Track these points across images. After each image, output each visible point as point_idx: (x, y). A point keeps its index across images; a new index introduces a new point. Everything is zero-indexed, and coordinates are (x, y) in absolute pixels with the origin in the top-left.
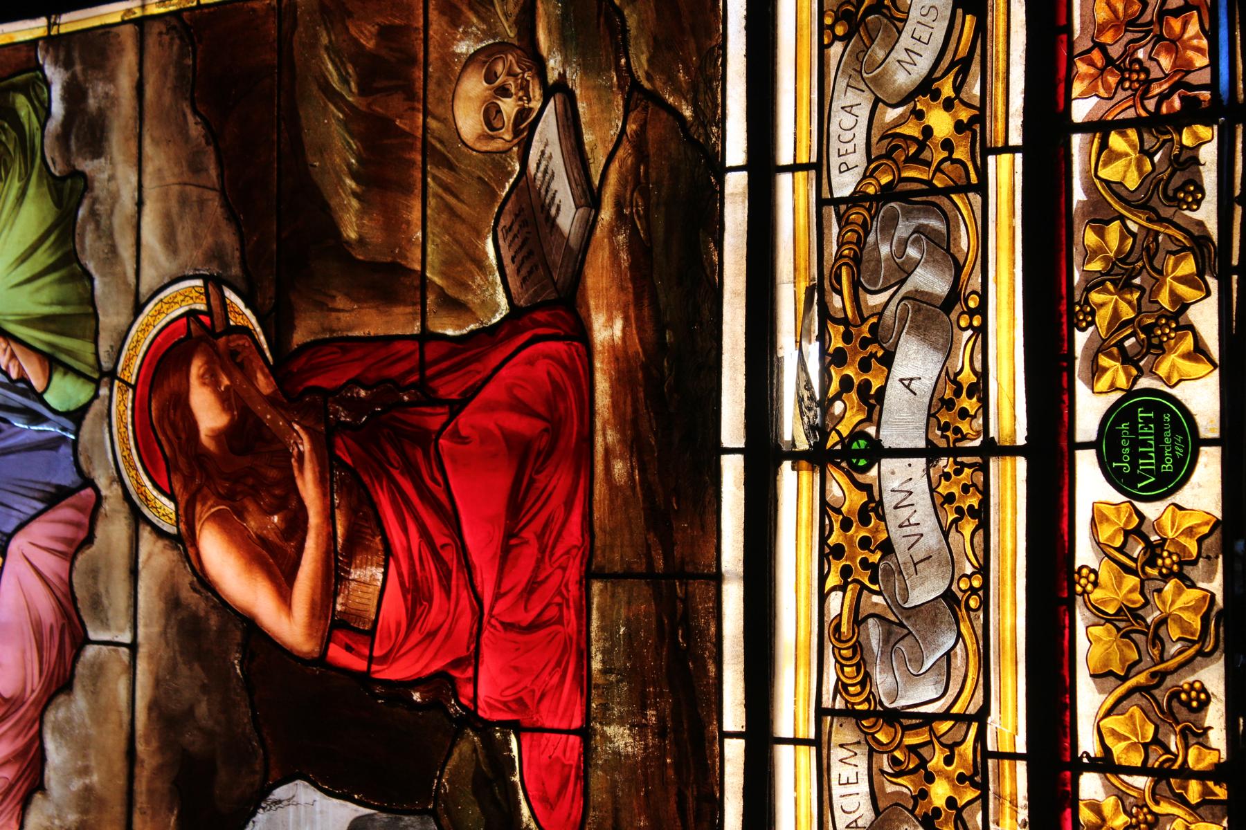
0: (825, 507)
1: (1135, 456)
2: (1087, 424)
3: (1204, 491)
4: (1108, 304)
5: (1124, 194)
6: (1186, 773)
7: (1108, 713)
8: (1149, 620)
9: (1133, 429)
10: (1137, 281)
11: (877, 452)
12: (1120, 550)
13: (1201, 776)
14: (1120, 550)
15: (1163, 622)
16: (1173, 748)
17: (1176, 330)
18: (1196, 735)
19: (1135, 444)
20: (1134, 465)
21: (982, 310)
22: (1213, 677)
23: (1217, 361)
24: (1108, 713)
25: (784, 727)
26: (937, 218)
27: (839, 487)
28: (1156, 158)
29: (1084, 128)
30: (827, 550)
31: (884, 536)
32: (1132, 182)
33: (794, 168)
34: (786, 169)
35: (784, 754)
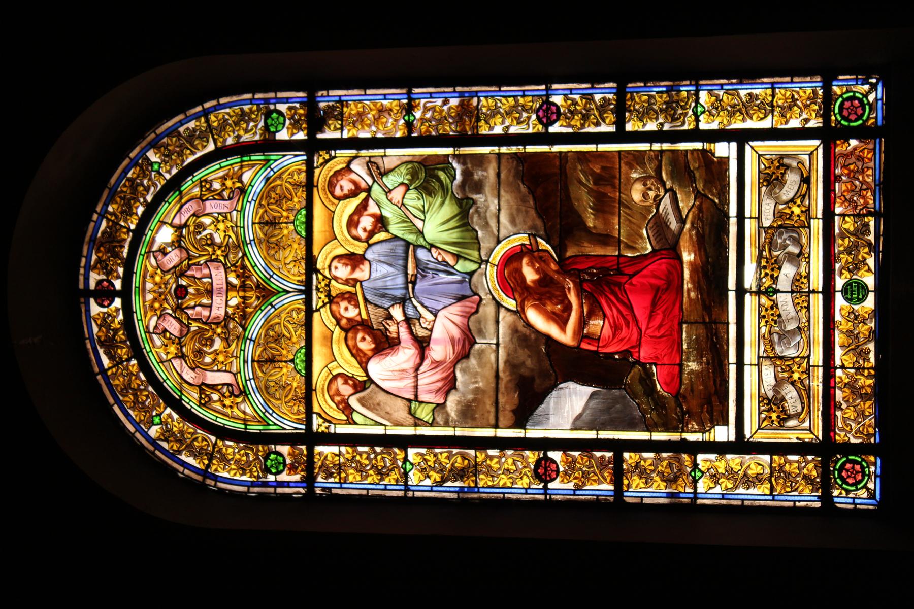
3: (870, 303)
6: (864, 369)
18: (867, 360)
22: (871, 346)
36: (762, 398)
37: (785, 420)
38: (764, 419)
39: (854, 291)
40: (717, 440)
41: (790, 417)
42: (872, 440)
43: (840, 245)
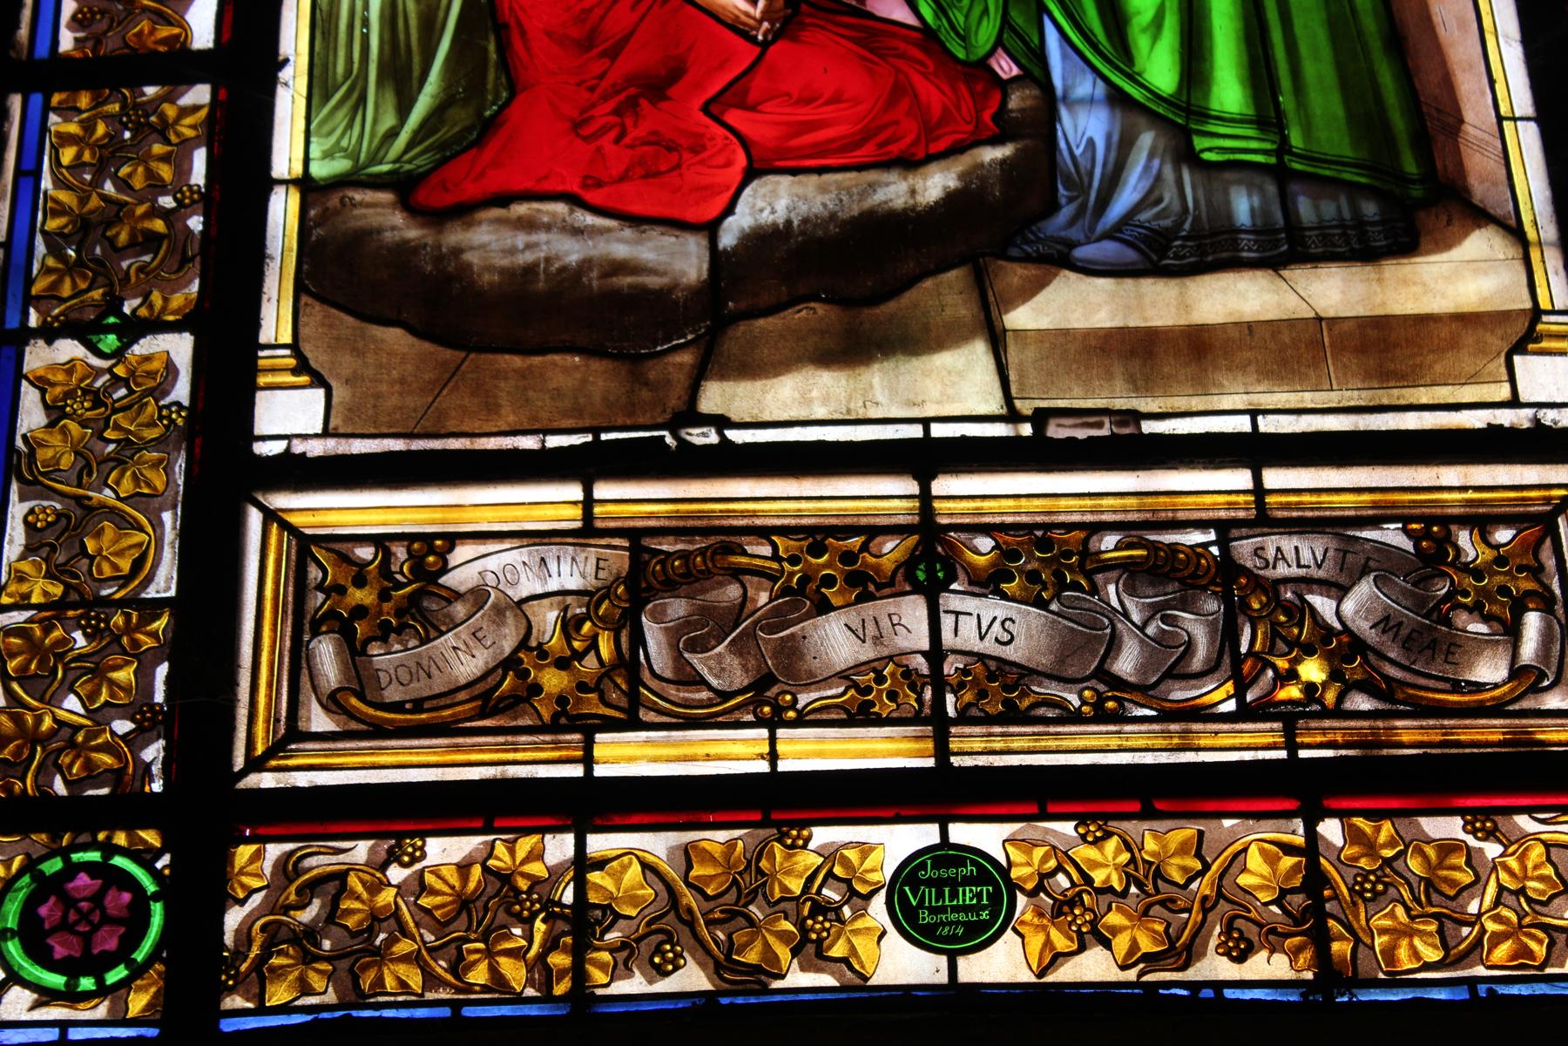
1: (938, 884)
3: (902, 963)
4: (1106, 862)
5: (1233, 870)
6: (579, 953)
7: (645, 866)
8: (751, 907)
9: (968, 881)
10: (1133, 890)
11: (932, 593)
12: (830, 874)
13: (579, 973)
14: (830, 874)
15: (751, 922)
16: (607, 937)
17: (1079, 932)
18: (625, 957)
19: (954, 884)
20: (930, 883)
21: (1101, 716)
22: (692, 978)
23: (1049, 979)
24: (645, 866)
26: (1207, 660)
28: (1274, 908)
29: (1311, 834)
30: (819, 538)
31: (836, 601)
32: (1244, 880)
33: (926, 497)
34: (1257, 479)
36: (433, 548)
37: (345, 632)
38: (345, 559)
39: (943, 901)
40: (261, 397)
41: (354, 652)
42: (236, 1002)
43: (1164, 840)
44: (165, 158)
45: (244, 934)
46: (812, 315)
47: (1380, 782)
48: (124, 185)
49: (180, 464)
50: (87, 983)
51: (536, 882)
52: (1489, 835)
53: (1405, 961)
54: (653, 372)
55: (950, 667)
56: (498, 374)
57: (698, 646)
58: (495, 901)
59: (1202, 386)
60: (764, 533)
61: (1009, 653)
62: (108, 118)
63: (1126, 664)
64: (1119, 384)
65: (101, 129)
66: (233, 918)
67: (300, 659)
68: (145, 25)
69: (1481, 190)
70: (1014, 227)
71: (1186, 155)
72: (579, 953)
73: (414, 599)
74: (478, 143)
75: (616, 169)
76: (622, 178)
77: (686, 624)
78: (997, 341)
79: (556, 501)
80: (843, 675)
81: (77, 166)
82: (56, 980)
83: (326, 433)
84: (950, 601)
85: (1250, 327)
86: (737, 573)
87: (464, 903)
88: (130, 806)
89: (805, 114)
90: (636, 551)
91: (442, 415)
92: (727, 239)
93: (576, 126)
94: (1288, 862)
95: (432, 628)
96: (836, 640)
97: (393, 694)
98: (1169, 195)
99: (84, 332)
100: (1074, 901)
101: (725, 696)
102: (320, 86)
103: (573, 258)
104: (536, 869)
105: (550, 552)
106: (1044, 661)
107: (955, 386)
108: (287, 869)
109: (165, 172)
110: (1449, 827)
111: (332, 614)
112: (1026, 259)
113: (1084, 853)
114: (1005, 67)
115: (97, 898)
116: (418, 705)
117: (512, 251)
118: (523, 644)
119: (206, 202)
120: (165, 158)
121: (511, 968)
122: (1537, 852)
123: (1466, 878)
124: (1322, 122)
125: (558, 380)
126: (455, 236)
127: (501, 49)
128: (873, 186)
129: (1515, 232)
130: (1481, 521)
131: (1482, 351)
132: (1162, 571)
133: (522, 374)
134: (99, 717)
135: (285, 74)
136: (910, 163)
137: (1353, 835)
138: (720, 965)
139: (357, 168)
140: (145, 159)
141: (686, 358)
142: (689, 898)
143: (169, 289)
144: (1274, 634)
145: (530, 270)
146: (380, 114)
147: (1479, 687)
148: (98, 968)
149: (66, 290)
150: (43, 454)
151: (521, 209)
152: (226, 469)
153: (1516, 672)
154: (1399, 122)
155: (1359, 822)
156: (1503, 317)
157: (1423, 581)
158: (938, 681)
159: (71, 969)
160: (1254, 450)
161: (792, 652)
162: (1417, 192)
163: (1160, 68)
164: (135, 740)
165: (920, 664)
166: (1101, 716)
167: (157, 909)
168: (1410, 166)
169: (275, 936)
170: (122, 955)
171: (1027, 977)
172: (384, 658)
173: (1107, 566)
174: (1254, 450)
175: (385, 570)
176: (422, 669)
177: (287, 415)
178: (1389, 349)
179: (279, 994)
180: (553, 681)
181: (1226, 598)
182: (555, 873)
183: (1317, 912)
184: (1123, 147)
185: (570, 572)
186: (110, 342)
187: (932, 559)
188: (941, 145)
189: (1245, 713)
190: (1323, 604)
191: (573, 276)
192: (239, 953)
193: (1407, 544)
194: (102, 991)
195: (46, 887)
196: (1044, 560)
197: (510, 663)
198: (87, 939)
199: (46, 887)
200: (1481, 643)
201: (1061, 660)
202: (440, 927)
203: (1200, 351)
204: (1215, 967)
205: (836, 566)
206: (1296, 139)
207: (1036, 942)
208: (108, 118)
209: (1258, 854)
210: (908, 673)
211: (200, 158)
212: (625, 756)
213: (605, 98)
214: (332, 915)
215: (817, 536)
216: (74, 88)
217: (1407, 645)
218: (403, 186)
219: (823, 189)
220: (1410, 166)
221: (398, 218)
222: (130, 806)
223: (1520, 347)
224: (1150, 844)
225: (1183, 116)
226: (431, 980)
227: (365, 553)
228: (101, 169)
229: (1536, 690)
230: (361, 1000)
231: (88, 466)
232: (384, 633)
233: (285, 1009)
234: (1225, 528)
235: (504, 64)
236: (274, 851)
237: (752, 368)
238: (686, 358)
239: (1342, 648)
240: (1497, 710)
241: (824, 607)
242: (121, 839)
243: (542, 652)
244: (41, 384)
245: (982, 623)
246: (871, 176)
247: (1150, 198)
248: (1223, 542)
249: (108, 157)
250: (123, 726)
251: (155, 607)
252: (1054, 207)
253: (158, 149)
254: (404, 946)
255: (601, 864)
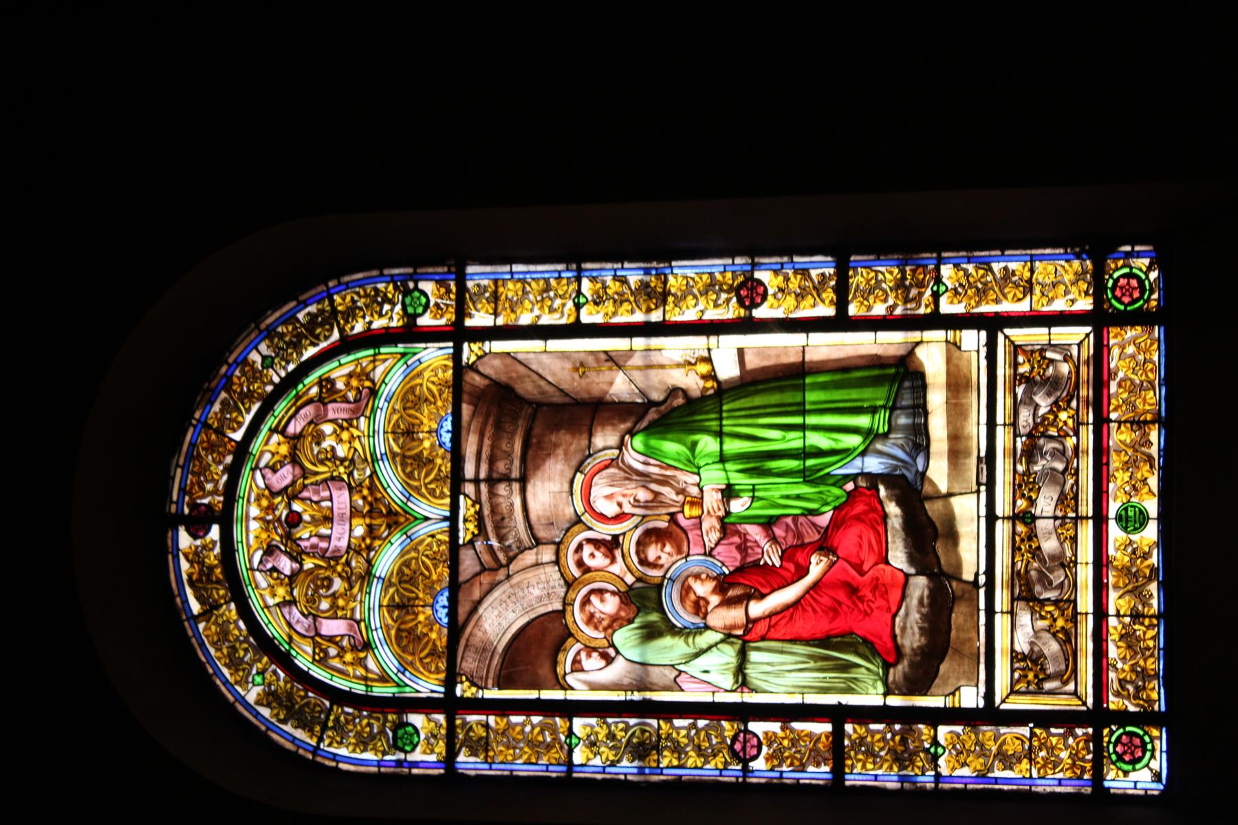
0: (1014, 533)
1: (1127, 522)
2: (1112, 513)
3: (1150, 533)
4: (1122, 477)
6: (1144, 616)
11: (1034, 518)
22: (1153, 587)
25: (998, 608)
27: (1020, 528)
32: (1128, 441)
35: (998, 617)
36: (1015, 656)
41: (1049, 678)
43: (1115, 462)
44: (873, 737)
45: (1137, 705)
46: (940, 548)
47: (1099, 403)
48: (882, 749)
49: (985, 728)
50: (1149, 747)
51: (1123, 628)
52: (1116, 374)
53: (1154, 401)
54: (959, 593)
55: (1059, 514)
56: (958, 638)
57: (1050, 583)
58: (1128, 637)
59: (969, 438)
60: (1013, 564)
61: (1055, 498)
62: (856, 754)
63: (1060, 466)
64: (967, 461)
65: (860, 757)
66: (1132, 708)
67: (1051, 693)
68: (820, 746)
69: (901, 351)
70: (911, 490)
71: (885, 436)
72: (1144, 616)
73: (1032, 661)
74: (872, 644)
75: (884, 603)
76: (888, 601)
77: (1043, 586)
78: (951, 494)
79: (1002, 623)
80: (1061, 544)
81: (874, 763)
82: (1148, 754)
83: (977, 686)
84: (1038, 513)
85: (949, 422)
86: (1027, 571)
87: (1129, 647)
88: (1097, 738)
89: (865, 546)
90: (1018, 599)
91: (972, 654)
92: (912, 571)
93: (866, 614)
94: (1123, 428)
95: (1042, 655)
96: (1049, 545)
97: (1063, 667)
98: (900, 442)
99: (935, 757)
100: (1134, 486)
101: (1067, 576)
102: (849, 690)
103: (917, 616)
104: (1120, 627)
105: (1018, 623)
106: (1058, 489)
107: (967, 510)
108: (1118, 694)
109: (878, 737)
110: (1113, 387)
111: (1037, 684)
112: (922, 484)
113: (1119, 483)
114: (850, 486)
115: (1124, 745)
116: (1067, 660)
117: (913, 634)
118: (1049, 631)
119: (890, 723)
120: (873, 737)
121: (1151, 636)
122: (1122, 363)
123: (1129, 383)
124: (877, 395)
125: (961, 620)
126: (907, 650)
127: (837, 636)
128: (893, 528)
129: (917, 344)
130: (1016, 365)
131: (960, 358)
132: (1030, 453)
133: (958, 630)
134: (1067, 747)
135: (844, 702)
136: (885, 516)
137: (1115, 410)
138: (1150, 580)
139: (881, 679)
140: (873, 743)
141: (954, 584)
142: (1130, 587)
143: (921, 733)
144: (1052, 425)
145: (921, 628)
146: (860, 674)
147: (1070, 372)
148: (1144, 744)
149: (920, 764)
150: (979, 767)
151: (898, 631)
152: (990, 714)
153: (1065, 360)
154: (875, 372)
155: (1112, 407)
156: (948, 351)
157: (1035, 383)
158: (1064, 517)
159: (1144, 751)
160: (1100, 613)
161: (1053, 557)
162: (901, 370)
163: (854, 441)
164: (1075, 737)
165: (1058, 522)
166: (1077, 473)
167: (1129, 729)
168: (892, 371)
169: (1136, 697)
170: (1141, 738)
171: (1156, 500)
172: (1051, 669)
173: (1028, 469)
174: (1100, 613)
175: (1023, 669)
176: (1055, 659)
177: (970, 698)
178: (957, 385)
179: (1154, 696)
180: (1060, 623)
181: (1039, 438)
182: (1120, 622)
183: (1138, 423)
184: (881, 453)
185: (1024, 618)
186: (940, 750)
187: (1026, 518)
188: (879, 508)
189: (1077, 434)
190: (1042, 411)
191: (924, 617)
192: (1142, 706)
193: (1023, 386)
194: (1152, 741)
195: (1120, 758)
196: (1025, 485)
197: (1054, 635)
198: (1136, 747)
199: (1120, 758)
200: (1056, 369)
201: (1058, 483)
202: (1136, 653)
203: (956, 438)
204: (1154, 450)
205: (1025, 543)
206: (881, 403)
207: (1145, 496)
208: (856, 754)
209: (1119, 437)
210: (1061, 525)
211: (873, 727)
212: (1086, 602)
213: (856, 605)
214: (1131, 682)
215: (1015, 549)
216: (844, 766)
217: (1056, 389)
218: (887, 666)
219: (894, 542)
220: (892, 371)
221: (900, 667)
222: (1097, 738)
223: (959, 348)
224: (1117, 464)
225: (870, 435)
226: (1152, 655)
227: (1016, 675)
228: (875, 756)
229: (1071, 357)
230: (1157, 676)
231: (983, 753)
232: (1043, 669)
233: (1159, 693)
234: (1015, 436)
235: (843, 636)
236: (1111, 698)
237: (959, 565)
238: (954, 584)
239: (1056, 407)
240: (1077, 368)
241: (1039, 548)
242: (1106, 739)
243: (1051, 626)
244: (953, 769)
245: (1046, 503)
246: (889, 528)
247: (902, 447)
248: (1021, 436)
249: (870, 753)
250: (1071, 740)
251: (1033, 734)
252: (903, 476)
253: (869, 739)
254: (1142, 663)
255: (1118, 611)
